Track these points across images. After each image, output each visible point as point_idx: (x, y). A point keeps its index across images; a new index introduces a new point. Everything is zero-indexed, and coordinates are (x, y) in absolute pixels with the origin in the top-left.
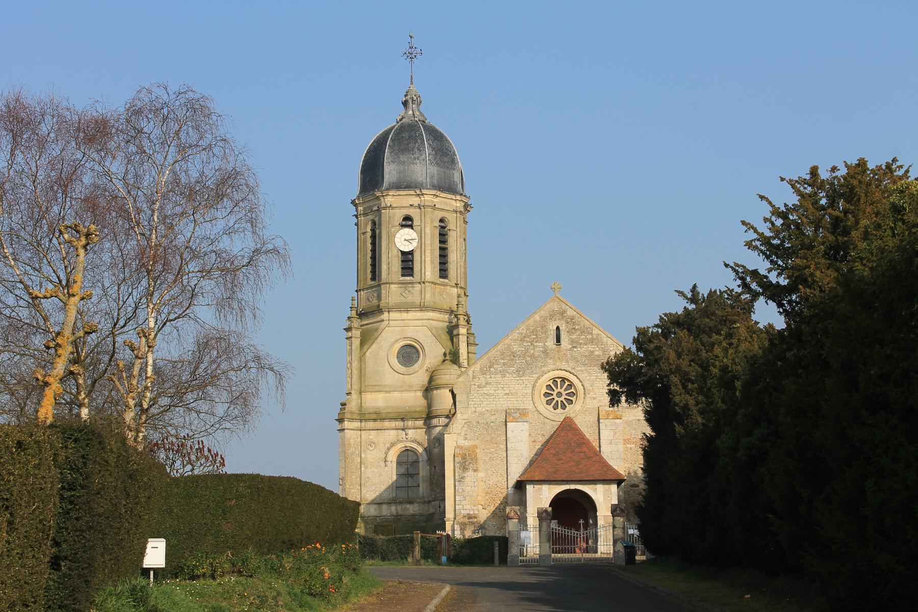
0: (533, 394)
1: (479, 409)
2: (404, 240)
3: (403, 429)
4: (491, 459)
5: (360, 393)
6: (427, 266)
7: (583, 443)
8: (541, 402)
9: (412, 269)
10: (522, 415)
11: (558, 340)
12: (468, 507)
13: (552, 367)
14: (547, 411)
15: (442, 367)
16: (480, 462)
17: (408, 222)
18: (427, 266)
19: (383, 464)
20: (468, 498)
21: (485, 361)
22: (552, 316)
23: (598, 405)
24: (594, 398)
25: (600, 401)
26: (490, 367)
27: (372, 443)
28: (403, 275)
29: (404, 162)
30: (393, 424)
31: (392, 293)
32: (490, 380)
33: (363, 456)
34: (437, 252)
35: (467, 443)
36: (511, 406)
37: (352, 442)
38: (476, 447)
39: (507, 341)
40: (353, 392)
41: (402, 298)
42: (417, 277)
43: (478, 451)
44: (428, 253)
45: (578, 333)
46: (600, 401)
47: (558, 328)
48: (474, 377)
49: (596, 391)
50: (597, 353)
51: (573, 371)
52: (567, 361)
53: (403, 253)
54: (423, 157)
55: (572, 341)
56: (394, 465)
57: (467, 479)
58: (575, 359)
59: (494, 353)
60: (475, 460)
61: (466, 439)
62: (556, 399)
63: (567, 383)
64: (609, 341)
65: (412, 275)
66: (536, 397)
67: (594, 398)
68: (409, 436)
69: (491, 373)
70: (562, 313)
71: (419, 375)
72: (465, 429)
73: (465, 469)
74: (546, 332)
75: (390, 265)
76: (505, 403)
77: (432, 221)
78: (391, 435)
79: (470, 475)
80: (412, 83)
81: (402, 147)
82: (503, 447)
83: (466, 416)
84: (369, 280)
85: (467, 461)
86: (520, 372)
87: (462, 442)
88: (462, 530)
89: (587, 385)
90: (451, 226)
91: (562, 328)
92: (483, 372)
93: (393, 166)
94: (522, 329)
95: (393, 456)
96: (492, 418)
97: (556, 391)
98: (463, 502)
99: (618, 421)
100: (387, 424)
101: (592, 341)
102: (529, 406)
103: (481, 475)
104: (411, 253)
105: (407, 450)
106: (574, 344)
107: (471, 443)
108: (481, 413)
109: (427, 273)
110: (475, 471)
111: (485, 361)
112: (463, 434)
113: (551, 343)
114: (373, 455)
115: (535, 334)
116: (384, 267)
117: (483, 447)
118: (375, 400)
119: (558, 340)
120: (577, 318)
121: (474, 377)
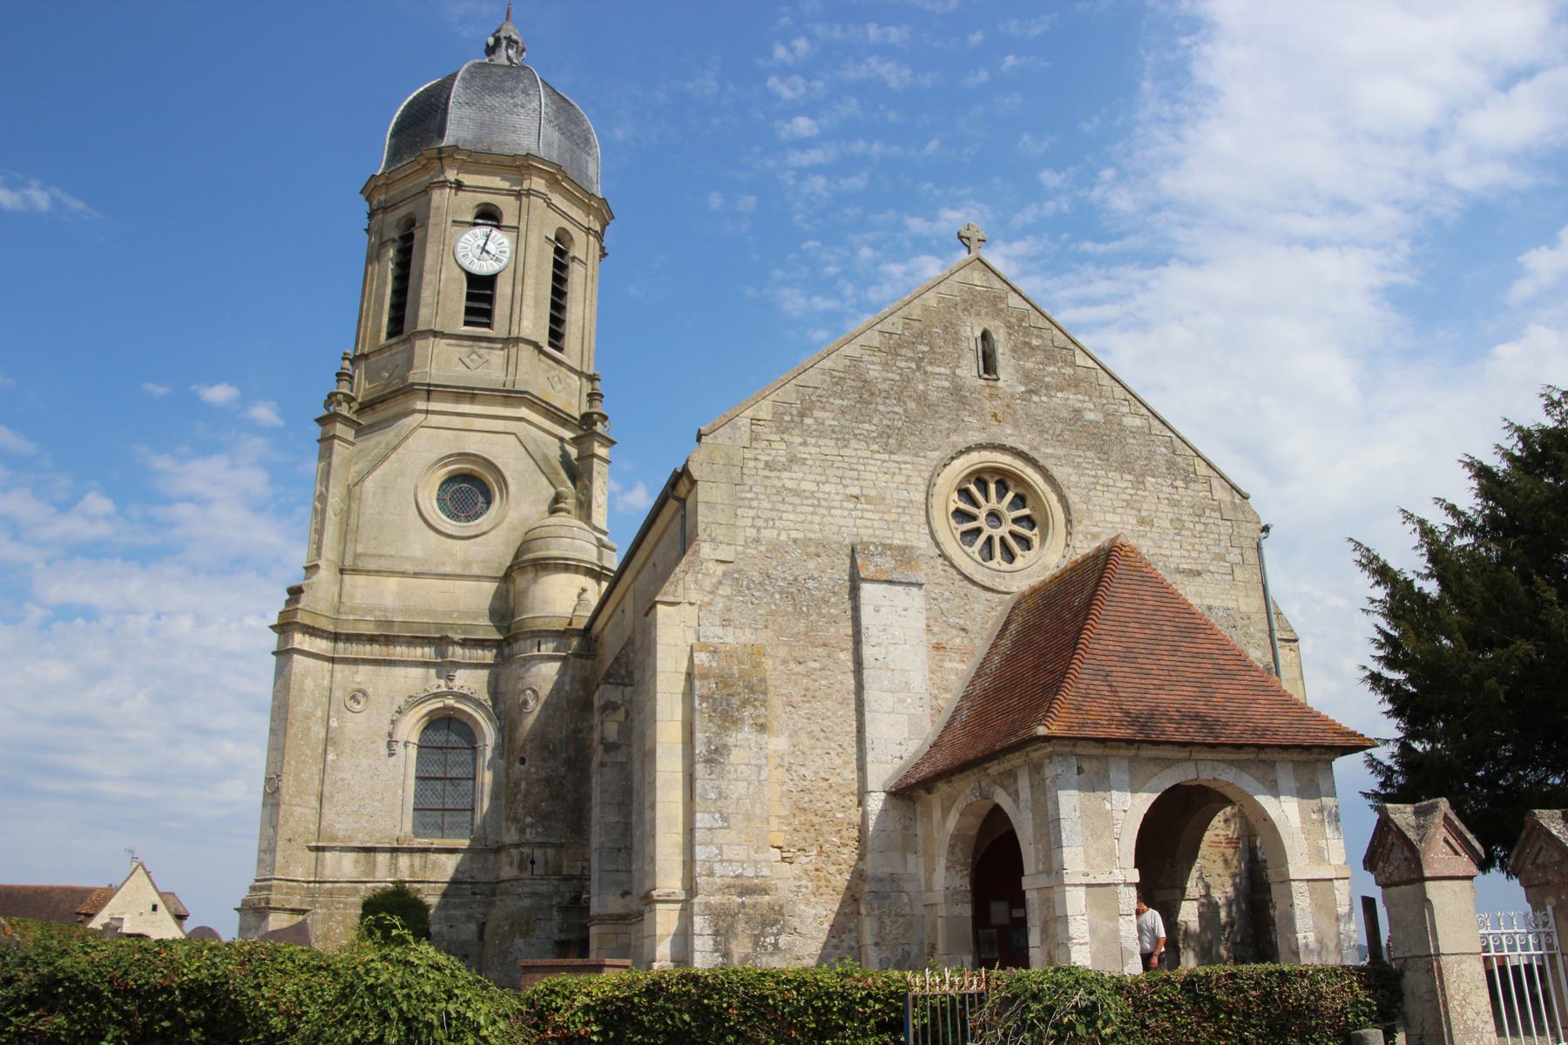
1: (768, 534)
2: (481, 250)
4: (809, 695)
8: (949, 532)
11: (989, 364)
12: (738, 852)
14: (967, 558)
16: (776, 702)
17: (489, 215)
26: (802, 415)
27: (358, 695)
28: (467, 323)
29: (493, 108)
30: (419, 653)
31: (439, 361)
32: (802, 452)
33: (334, 723)
34: (549, 268)
35: (732, 638)
36: (866, 534)
37: (309, 684)
38: (757, 652)
40: (322, 563)
41: (461, 368)
42: (499, 329)
43: (768, 663)
44: (529, 281)
45: (1040, 357)
47: (985, 336)
49: (1098, 517)
50: (1090, 416)
51: (1033, 454)
52: (1016, 426)
54: (535, 104)
55: (1027, 377)
56: (413, 752)
57: (736, 756)
58: (1037, 425)
59: (812, 377)
60: (756, 691)
61: (726, 623)
65: (489, 325)
69: (806, 432)
72: (725, 590)
73: (727, 718)
75: (442, 299)
78: (413, 679)
79: (742, 740)
81: (491, 83)
82: (846, 657)
83: (725, 553)
84: (384, 334)
85: (728, 697)
86: (891, 440)
87: (714, 633)
88: (722, 935)
89: (1073, 498)
90: (577, 251)
92: (782, 425)
93: (468, 111)
95: (410, 728)
96: (811, 564)
97: (982, 514)
98: (721, 836)
100: (400, 652)
101: (1074, 384)
103: (778, 743)
104: (489, 281)
106: (1033, 384)
107: (747, 637)
108: (775, 548)
109: (525, 323)
110: (762, 728)
112: (720, 605)
113: (969, 370)
114: (360, 725)
116: (427, 294)
118: (377, 597)
119: (989, 364)
121: (755, 437)
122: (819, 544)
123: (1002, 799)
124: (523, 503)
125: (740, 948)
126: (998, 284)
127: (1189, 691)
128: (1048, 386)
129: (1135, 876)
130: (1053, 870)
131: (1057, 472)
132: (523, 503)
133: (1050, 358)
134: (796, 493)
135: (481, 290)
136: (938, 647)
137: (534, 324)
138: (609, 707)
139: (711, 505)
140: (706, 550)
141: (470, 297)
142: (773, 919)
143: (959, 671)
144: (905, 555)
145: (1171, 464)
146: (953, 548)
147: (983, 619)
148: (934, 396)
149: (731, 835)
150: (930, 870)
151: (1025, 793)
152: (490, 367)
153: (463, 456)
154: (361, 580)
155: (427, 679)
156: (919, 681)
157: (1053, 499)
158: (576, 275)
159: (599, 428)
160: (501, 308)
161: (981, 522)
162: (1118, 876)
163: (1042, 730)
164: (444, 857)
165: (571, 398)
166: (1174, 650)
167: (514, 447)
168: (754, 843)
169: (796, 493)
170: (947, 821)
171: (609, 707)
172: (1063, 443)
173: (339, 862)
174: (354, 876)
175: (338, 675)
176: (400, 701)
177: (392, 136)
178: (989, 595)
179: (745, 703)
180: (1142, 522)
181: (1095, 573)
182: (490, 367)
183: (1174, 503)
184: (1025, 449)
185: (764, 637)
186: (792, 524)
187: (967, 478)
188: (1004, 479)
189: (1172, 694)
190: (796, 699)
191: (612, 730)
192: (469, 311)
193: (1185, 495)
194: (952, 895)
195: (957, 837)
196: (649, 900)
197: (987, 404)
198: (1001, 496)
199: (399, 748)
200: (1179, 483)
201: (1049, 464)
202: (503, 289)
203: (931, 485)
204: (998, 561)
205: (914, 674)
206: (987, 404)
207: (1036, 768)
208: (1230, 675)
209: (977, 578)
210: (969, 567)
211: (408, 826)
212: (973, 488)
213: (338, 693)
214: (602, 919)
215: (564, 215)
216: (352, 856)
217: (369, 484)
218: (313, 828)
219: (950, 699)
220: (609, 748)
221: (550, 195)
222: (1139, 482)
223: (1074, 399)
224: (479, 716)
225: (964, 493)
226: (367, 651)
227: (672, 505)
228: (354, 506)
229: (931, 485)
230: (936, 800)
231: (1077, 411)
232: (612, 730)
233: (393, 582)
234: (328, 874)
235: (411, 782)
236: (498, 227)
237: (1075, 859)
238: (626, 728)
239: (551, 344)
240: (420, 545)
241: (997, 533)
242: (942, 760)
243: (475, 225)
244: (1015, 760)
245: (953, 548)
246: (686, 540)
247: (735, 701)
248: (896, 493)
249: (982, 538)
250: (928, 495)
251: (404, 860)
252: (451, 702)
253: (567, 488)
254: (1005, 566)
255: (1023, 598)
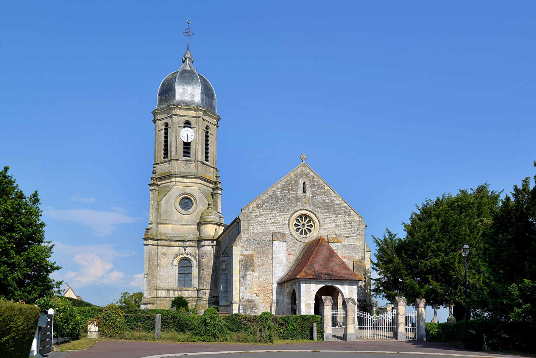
0: (289, 224)
1: (255, 231)
2: (187, 135)
3: (183, 247)
4: (263, 264)
5: (158, 224)
6: (198, 152)
7: (334, 255)
8: (293, 229)
9: (189, 153)
10: (282, 237)
11: (304, 191)
13: (300, 208)
14: (296, 235)
15: (208, 211)
16: (256, 266)
17: (187, 124)
18: (198, 152)
19: (171, 267)
20: (248, 289)
21: (259, 200)
22: (301, 175)
23: (327, 233)
24: (325, 229)
25: (328, 231)
26: (263, 205)
27: (164, 254)
28: (184, 156)
33: (159, 261)
35: (247, 253)
36: (275, 231)
39: (273, 189)
43: (255, 258)
44: (200, 144)
46: (328, 231)
47: (304, 183)
48: (253, 210)
49: (326, 225)
50: (327, 201)
51: (313, 211)
53: (185, 144)
55: (313, 193)
56: (177, 267)
57: (248, 276)
59: (265, 196)
60: (252, 264)
62: (302, 228)
63: (308, 219)
64: (334, 195)
65: (189, 157)
66: (291, 226)
67: (325, 229)
68: (187, 251)
69: (263, 208)
70: (307, 174)
71: (193, 215)
72: (246, 243)
74: (297, 185)
75: (176, 149)
76: (275, 229)
77: (202, 126)
80: (188, 49)
83: (247, 235)
85: (248, 264)
86: (281, 209)
87: (244, 252)
89: (321, 221)
91: (307, 183)
94: (284, 182)
95: (176, 262)
99: (339, 244)
100: (173, 243)
101: (324, 193)
102: (286, 231)
103: (256, 274)
104: (189, 144)
105: (185, 260)
106: (314, 194)
107: (250, 253)
108: (257, 234)
109: (199, 156)
110: (253, 271)
111: (259, 200)
113: (300, 192)
114: (163, 261)
115: (290, 186)
117: (257, 256)
118: (165, 229)
119: (304, 191)
120: (316, 178)
121: (253, 210)
122: (266, 233)
123: (294, 287)
124: (200, 206)
125: (248, 312)
126: (241, 307)
127: (329, 268)
128: (318, 195)
129: (314, 302)
130: (300, 299)
131: (318, 215)
132: (200, 206)
133: (319, 188)
134: (261, 222)
135: (187, 146)
136: (289, 254)
137: (201, 156)
138: (224, 261)
139: (244, 226)
140: (243, 235)
141: (184, 148)
142: (255, 306)
143: (293, 259)
144: (283, 235)
145: (345, 212)
146: (294, 233)
147: (299, 248)
148: (291, 199)
149: (247, 291)
150: (284, 298)
151: (297, 286)
152: (192, 168)
153: (185, 193)
154: (162, 226)
155: (180, 250)
156: (284, 261)
157: (317, 220)
158: (211, 138)
159: (219, 186)
160: (192, 152)
161: (301, 227)
162: (311, 302)
163: (298, 277)
164: (185, 292)
165: (211, 175)
166: (328, 260)
167: (194, 188)
168: (254, 291)
169: (261, 222)
170: (287, 290)
171: (224, 261)
172: (320, 208)
173: (162, 293)
174: (165, 296)
175: (159, 249)
176: (174, 255)
177: (159, 95)
178: (301, 243)
179: (250, 266)
180: (337, 225)
181: (317, 242)
182: (192, 168)
183: (345, 221)
184: (311, 210)
185: (254, 253)
186: (260, 229)
187: (298, 217)
188: (306, 216)
189: (324, 268)
190: (260, 265)
191: (224, 266)
192: (184, 152)
193: (348, 219)
194: (288, 303)
195: (289, 293)
196: (232, 303)
197: (304, 200)
198: (304, 222)
199: (174, 267)
200: (347, 216)
201: (316, 213)
202: (193, 146)
203: (290, 219)
204: (303, 235)
205: (283, 259)
206: (304, 200)
207: (299, 282)
208: (338, 265)
209: (298, 239)
210: (297, 237)
211: (177, 285)
212: (299, 218)
213: (159, 254)
214: (222, 306)
215: (208, 121)
216: (165, 291)
217: (163, 201)
218: (156, 285)
219: (290, 265)
220: (223, 270)
221: (204, 117)
222: (337, 217)
223: (323, 197)
224: (192, 259)
225: (297, 220)
226: (165, 243)
227: (235, 223)
228: (160, 207)
229: (290, 219)
230: (285, 285)
231: (324, 200)
232: (224, 266)
233: (170, 226)
234: (159, 296)
235: (177, 274)
236: (190, 128)
237: (303, 298)
238: (227, 266)
239: (206, 160)
240: (176, 216)
241: (304, 229)
242: (286, 278)
243: (184, 127)
244: (296, 281)
245: (294, 233)
246: (239, 232)
247: (248, 266)
248: (283, 221)
249: (301, 230)
250: (289, 221)
251: (176, 292)
252: (185, 256)
253: (211, 202)
254: (305, 236)
255: (307, 244)
